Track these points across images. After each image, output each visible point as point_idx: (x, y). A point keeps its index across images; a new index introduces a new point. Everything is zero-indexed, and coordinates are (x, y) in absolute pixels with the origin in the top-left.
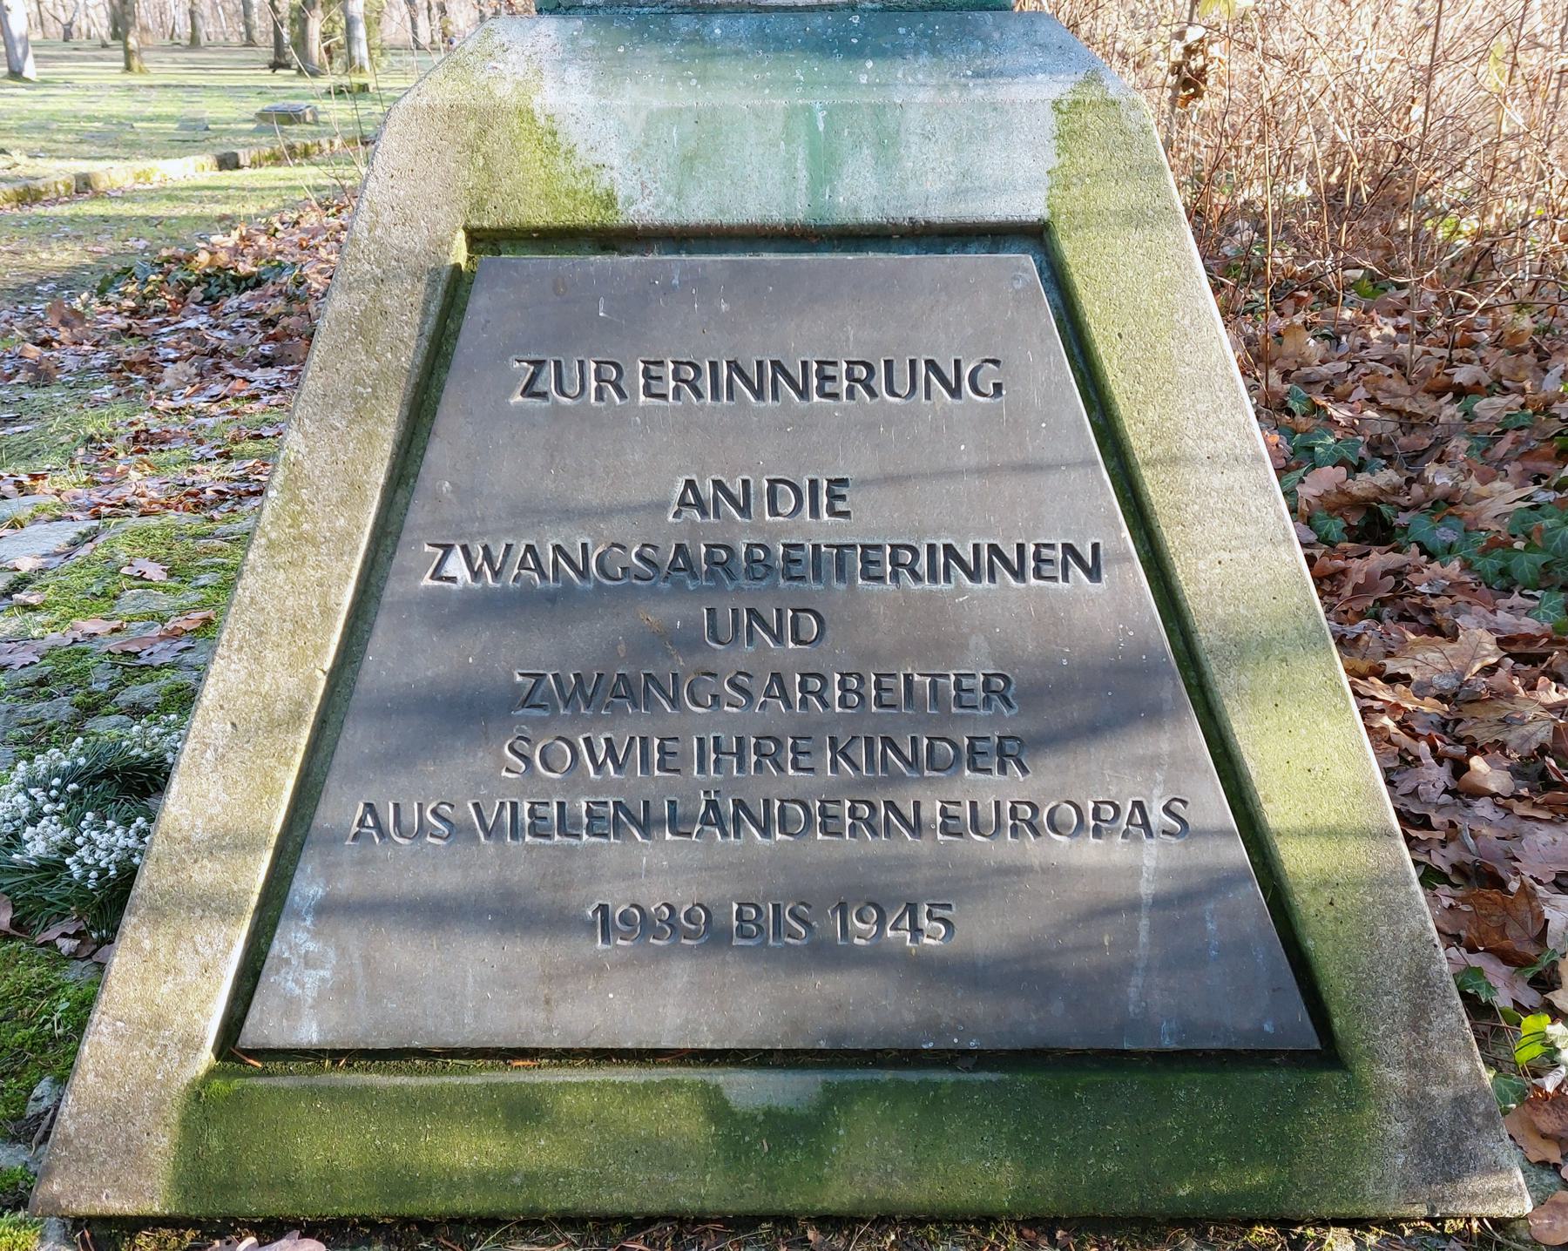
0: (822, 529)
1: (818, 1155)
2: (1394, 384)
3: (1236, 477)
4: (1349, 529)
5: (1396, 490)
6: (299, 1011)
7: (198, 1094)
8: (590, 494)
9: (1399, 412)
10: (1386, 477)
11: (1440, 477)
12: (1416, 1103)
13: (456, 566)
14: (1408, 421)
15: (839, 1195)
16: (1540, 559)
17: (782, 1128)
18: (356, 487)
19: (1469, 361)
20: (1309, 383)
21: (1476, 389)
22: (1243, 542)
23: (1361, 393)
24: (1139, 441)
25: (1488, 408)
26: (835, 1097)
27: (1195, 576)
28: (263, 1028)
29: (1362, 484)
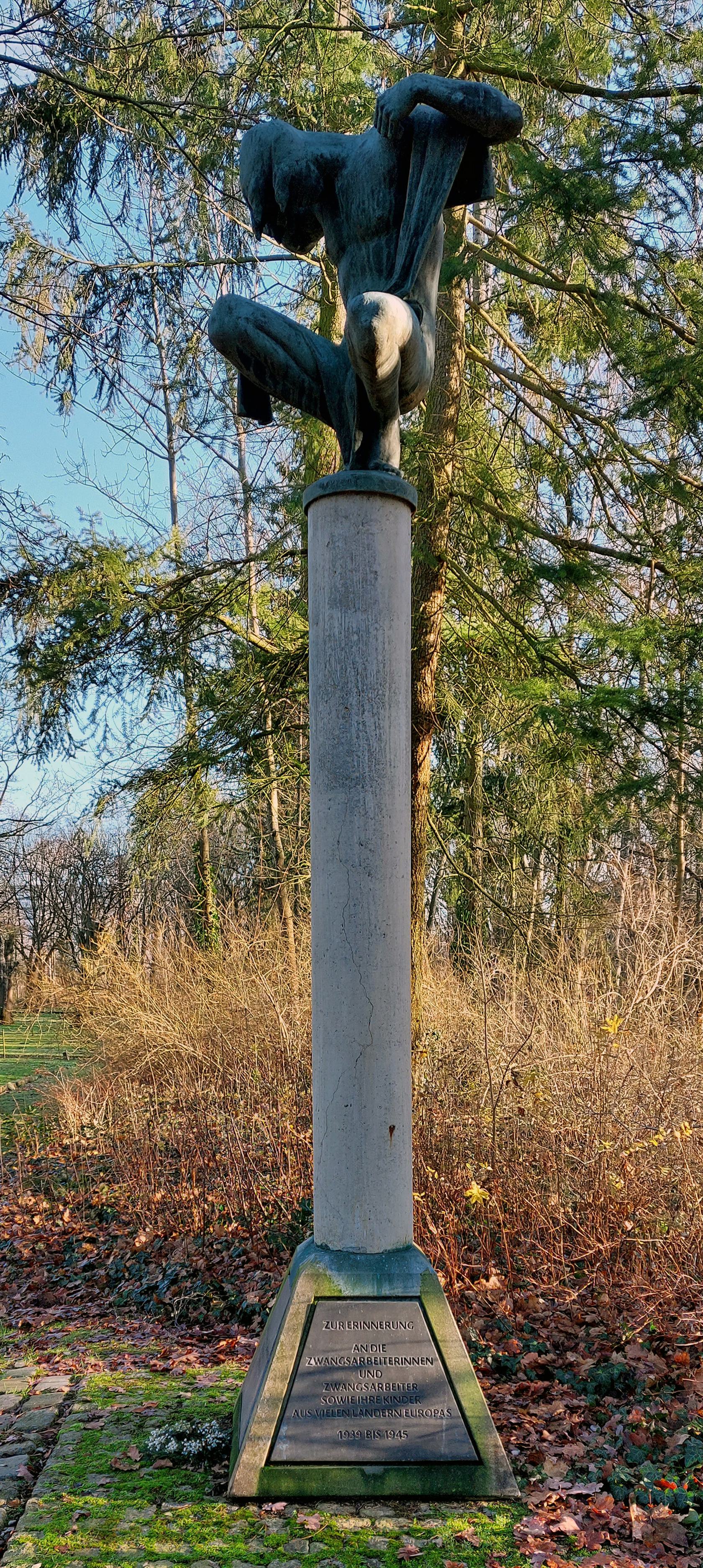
0: (381, 1355)
1: (383, 1483)
2: (565, 1321)
3: (457, 1344)
4: (537, 1375)
5: (554, 1361)
6: (284, 1451)
7: (262, 1469)
8: (338, 1347)
9: (566, 1333)
10: (551, 1356)
11: (571, 1357)
12: (497, 1472)
13: (313, 1362)
14: (568, 1335)
15: (387, 1492)
16: (594, 1384)
17: (375, 1477)
18: (294, 1347)
19: (594, 1312)
20: (534, 1320)
21: (594, 1324)
22: (459, 1359)
23: (553, 1325)
24: (438, 1338)
25: (593, 1331)
26: (386, 1471)
27: (450, 1363)
28: (274, 1458)
29: (542, 1360)
